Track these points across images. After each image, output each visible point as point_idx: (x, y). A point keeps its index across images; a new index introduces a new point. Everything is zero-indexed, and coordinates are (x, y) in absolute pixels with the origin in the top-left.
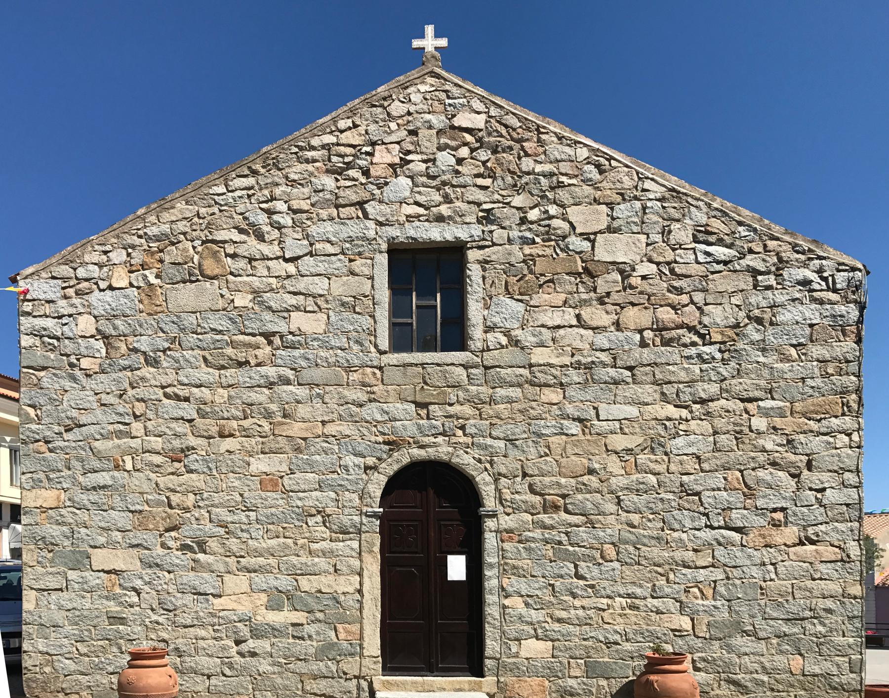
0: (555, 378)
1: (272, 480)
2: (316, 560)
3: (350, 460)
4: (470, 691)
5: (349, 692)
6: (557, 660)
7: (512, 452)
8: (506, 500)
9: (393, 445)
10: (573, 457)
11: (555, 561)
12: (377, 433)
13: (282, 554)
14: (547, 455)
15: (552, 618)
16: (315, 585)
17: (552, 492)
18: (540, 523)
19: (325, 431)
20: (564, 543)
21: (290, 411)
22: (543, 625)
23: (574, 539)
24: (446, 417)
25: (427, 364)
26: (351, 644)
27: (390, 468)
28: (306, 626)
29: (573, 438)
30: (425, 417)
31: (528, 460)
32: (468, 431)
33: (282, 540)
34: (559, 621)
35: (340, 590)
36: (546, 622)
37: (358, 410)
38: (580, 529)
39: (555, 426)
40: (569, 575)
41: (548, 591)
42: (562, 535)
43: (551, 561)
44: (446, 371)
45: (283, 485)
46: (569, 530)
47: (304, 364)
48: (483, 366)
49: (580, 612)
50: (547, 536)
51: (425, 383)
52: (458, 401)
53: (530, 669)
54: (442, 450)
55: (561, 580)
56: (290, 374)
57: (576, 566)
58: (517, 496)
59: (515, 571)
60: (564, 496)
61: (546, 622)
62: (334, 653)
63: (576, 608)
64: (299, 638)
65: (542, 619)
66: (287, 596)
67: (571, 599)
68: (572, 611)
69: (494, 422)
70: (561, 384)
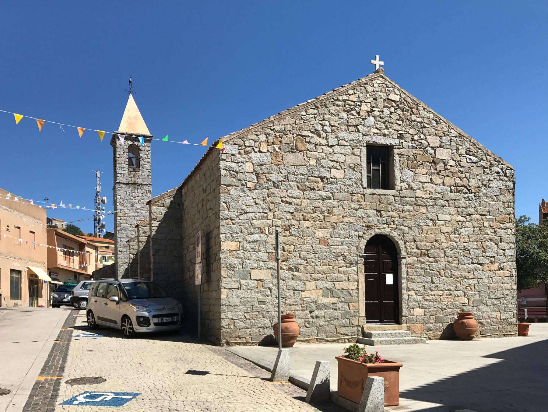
1: (324, 240)
3: (353, 233)
9: (369, 227)
10: (430, 235)
16: (341, 286)
23: (431, 268)
27: (368, 237)
32: (395, 223)
34: (427, 300)
41: (423, 288)
47: (336, 191)
51: (380, 202)
56: (330, 195)
70: (426, 205)
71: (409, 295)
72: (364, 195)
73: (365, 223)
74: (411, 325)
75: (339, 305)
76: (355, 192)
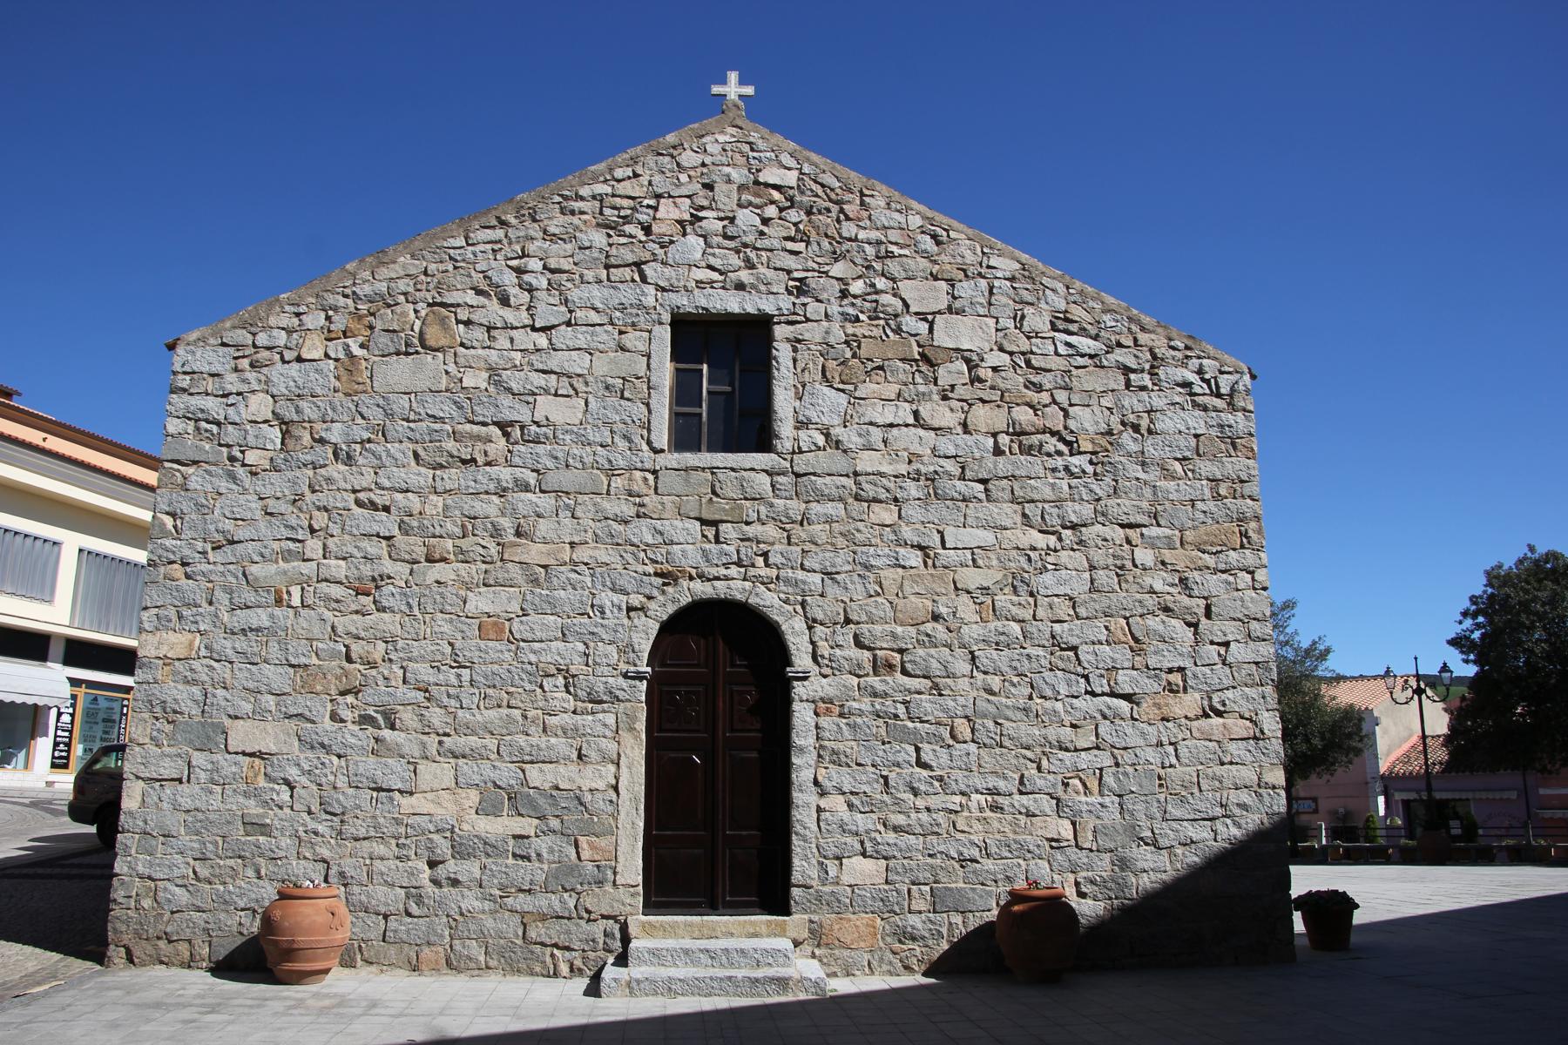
1: (495, 624)
2: (553, 740)
3: (607, 598)
4: (769, 936)
7: (832, 591)
8: (823, 657)
9: (669, 577)
10: (913, 598)
13: (504, 731)
16: (550, 777)
27: (663, 609)
32: (771, 560)
33: (505, 711)
34: (896, 829)
37: (621, 528)
41: (879, 787)
47: (550, 464)
49: (924, 817)
51: (714, 492)
53: (854, 901)
56: (532, 478)
57: (918, 750)
58: (838, 652)
60: (901, 651)
63: (918, 810)
64: (522, 857)
68: (913, 815)
71: (819, 810)
74: (826, 918)
75: (542, 844)
76: (622, 463)
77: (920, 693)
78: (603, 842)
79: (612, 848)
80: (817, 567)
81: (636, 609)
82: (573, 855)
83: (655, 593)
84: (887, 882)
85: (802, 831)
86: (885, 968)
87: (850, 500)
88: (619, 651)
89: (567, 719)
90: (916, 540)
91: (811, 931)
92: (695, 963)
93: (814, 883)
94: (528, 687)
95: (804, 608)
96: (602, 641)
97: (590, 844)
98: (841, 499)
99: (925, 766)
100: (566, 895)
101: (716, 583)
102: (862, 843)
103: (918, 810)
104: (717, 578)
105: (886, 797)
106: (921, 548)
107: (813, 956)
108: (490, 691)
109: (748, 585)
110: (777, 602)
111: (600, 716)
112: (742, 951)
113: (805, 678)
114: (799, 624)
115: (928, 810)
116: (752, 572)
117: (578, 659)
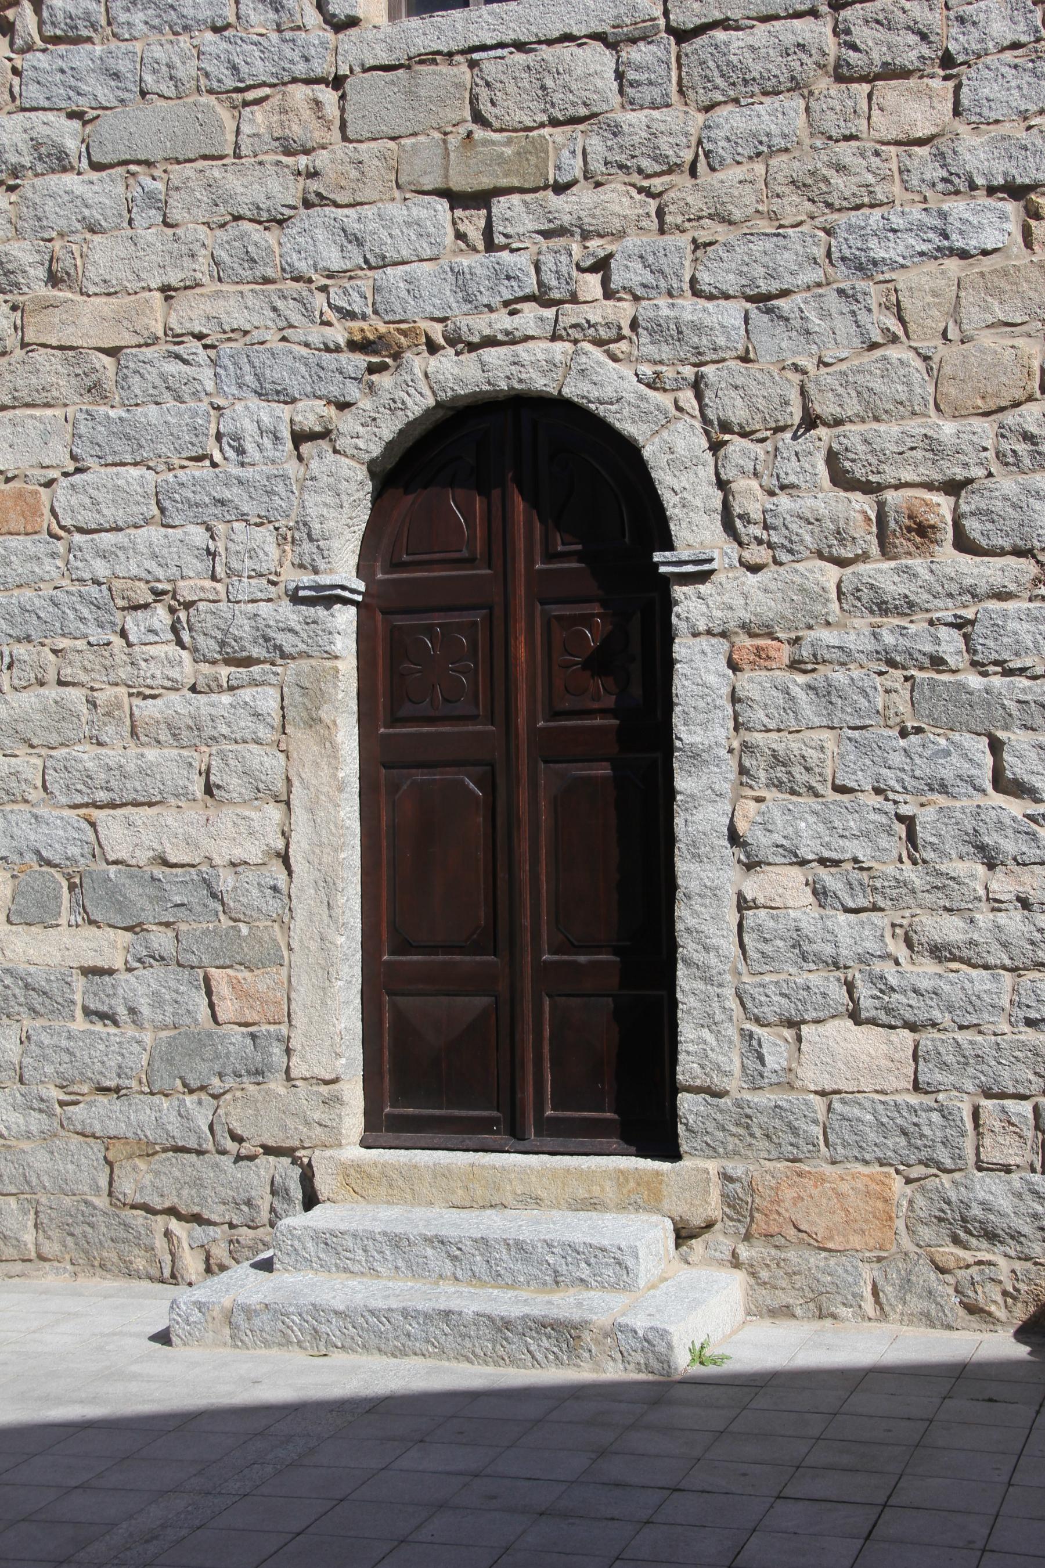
0: (924, 37)
1: (20, 495)
2: (152, 754)
3: (250, 415)
4: (622, 1208)
5: (249, 1203)
6: (928, 1100)
7: (773, 342)
8: (745, 518)
9: (378, 351)
10: (987, 340)
11: (919, 730)
12: (330, 315)
13: (54, 739)
14: (894, 339)
15: (909, 943)
16: (148, 838)
17: (908, 476)
18: (866, 594)
19: (173, 323)
20: (952, 661)
21: (68, 263)
22: (878, 966)
23: (988, 647)
24: (546, 234)
25: (484, 48)
26: (253, 1036)
27: (373, 427)
28: (123, 976)
29: (987, 263)
30: (481, 246)
31: (821, 363)
32: (617, 280)
33: (52, 692)
34: (939, 952)
35: (223, 852)
36: (887, 956)
37: (272, 238)
38: (1010, 605)
39: (921, 227)
40: (971, 781)
41: (895, 844)
42: (943, 632)
43: (904, 733)
44: (545, 66)
45: (53, 511)
46: (969, 614)
47: (105, 94)
48: (670, 30)
49: (1013, 921)
50: (889, 639)
51: (479, 118)
52: (587, 175)
53: (835, 1127)
54: (533, 364)
55: (942, 800)
56: (68, 135)
57: (996, 746)
58: (784, 501)
59: (780, 772)
60: (953, 488)
61: (887, 956)
62: (203, 1067)
63: (996, 905)
64: (103, 1016)
65: (871, 946)
66: (69, 877)
67: (981, 870)
68: (984, 917)
69: (703, 237)
70: (947, 61)
71: (743, 904)
72: (338, 82)
73: (349, 315)
74: (761, 1169)
75: (137, 988)
76: (261, 70)
77: (1003, 596)
78: (260, 982)
79: (281, 995)
80: (731, 283)
81: (313, 436)
82: (204, 1011)
83: (353, 392)
84: (916, 1087)
85: (699, 957)
86: (916, 1304)
87: (823, 84)
88: (281, 540)
89: (177, 704)
90: (1000, 171)
91: (730, 1201)
92: (417, 1269)
93: (732, 1084)
94: (97, 636)
95: (699, 396)
96: (243, 517)
97: (235, 985)
98: (796, 86)
99: (1018, 789)
100: (189, 1100)
101: (490, 354)
102: (850, 987)
103: (996, 905)
104: (490, 342)
105: (909, 871)
106: (1015, 191)
107: (736, 1263)
108: (21, 651)
109: (560, 349)
110: (630, 387)
111: (246, 694)
112: (520, 1247)
113: (703, 577)
114: (688, 439)
115: (1025, 903)
116: (571, 314)
117: (196, 566)
